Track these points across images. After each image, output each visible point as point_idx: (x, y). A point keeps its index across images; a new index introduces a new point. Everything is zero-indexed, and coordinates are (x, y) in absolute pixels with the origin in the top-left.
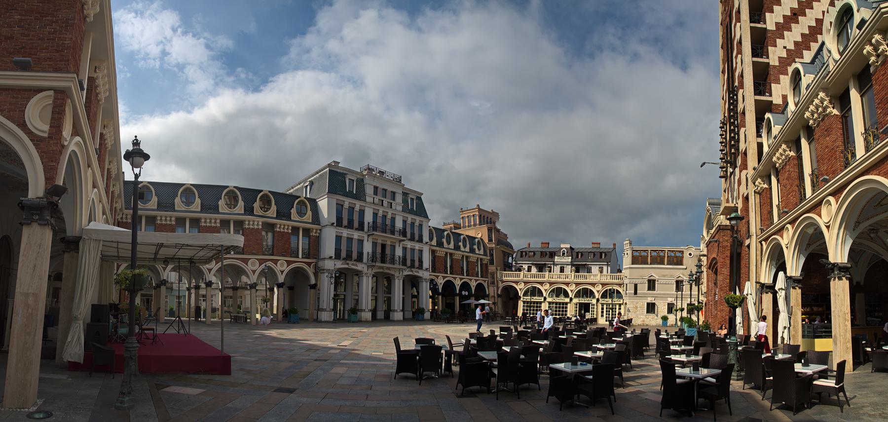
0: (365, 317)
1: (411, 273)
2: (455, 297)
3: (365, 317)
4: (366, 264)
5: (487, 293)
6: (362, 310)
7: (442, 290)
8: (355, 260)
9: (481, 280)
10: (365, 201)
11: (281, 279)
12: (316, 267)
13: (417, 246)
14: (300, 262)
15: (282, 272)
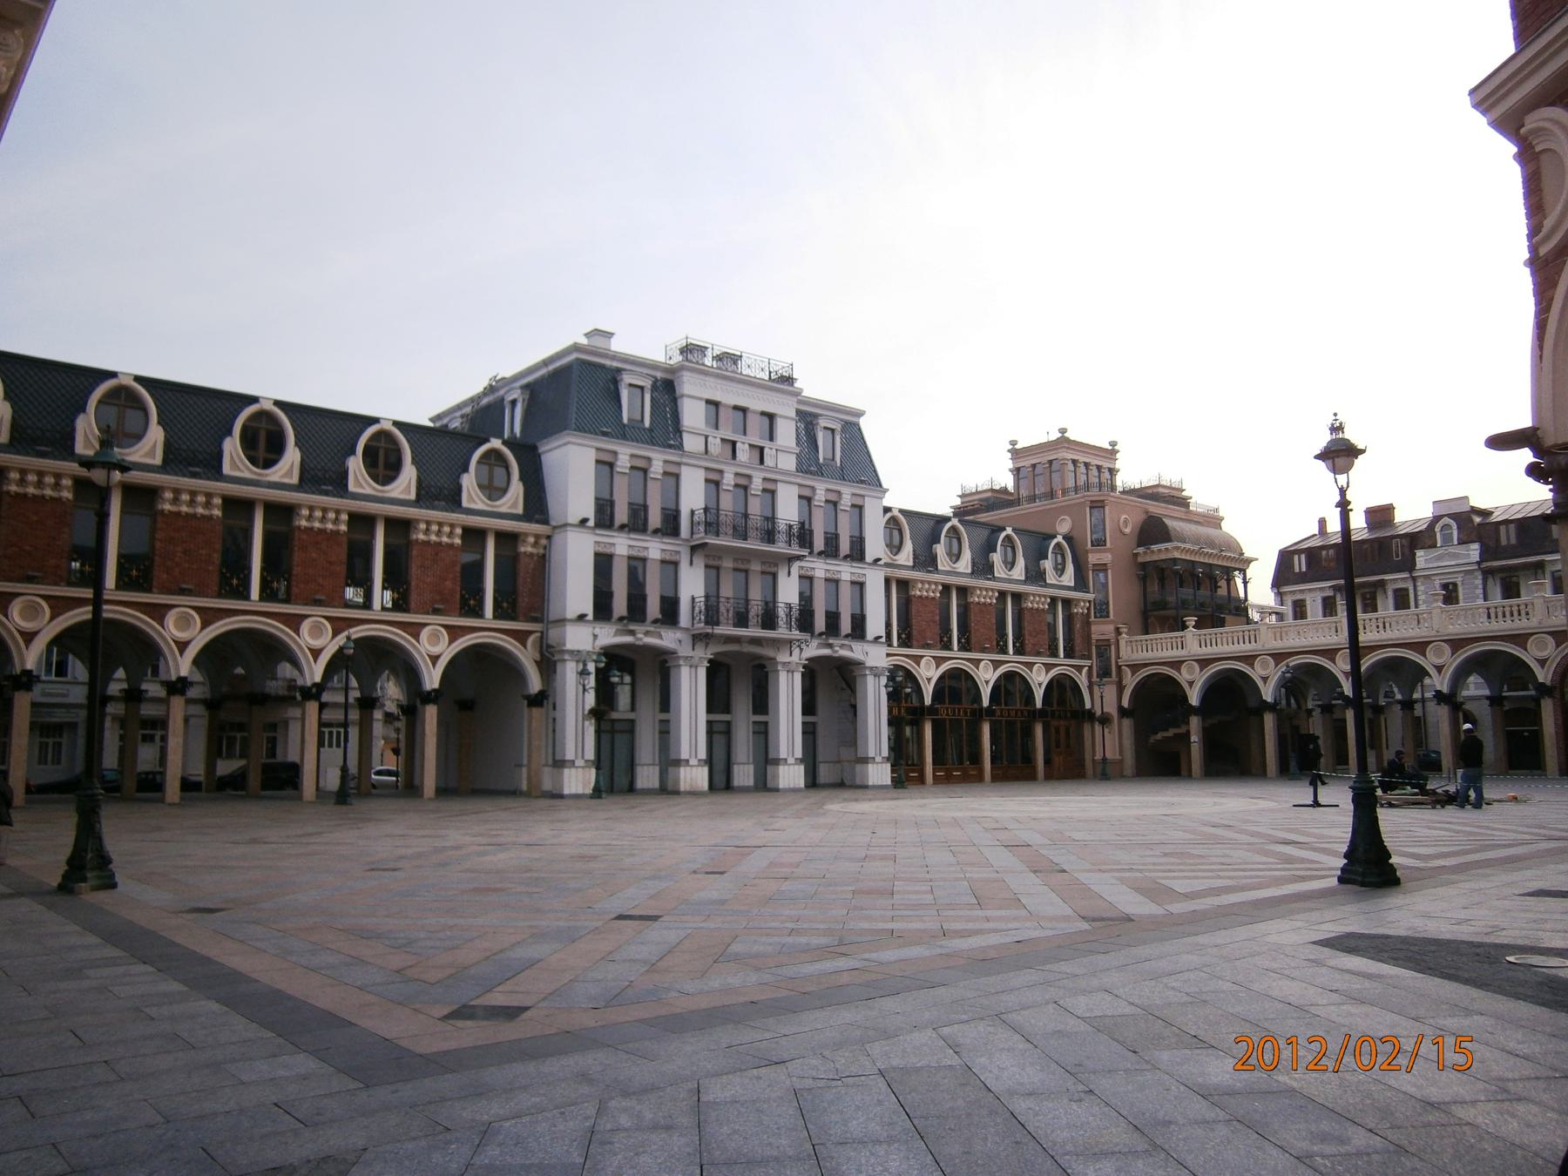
0: (688, 780)
1: (826, 652)
3: (688, 780)
4: (687, 629)
6: (868, 758)
7: (933, 700)
8: (655, 621)
9: (1063, 665)
10: (680, 447)
11: (432, 679)
12: (541, 647)
13: (846, 571)
14: (488, 630)
15: (435, 659)
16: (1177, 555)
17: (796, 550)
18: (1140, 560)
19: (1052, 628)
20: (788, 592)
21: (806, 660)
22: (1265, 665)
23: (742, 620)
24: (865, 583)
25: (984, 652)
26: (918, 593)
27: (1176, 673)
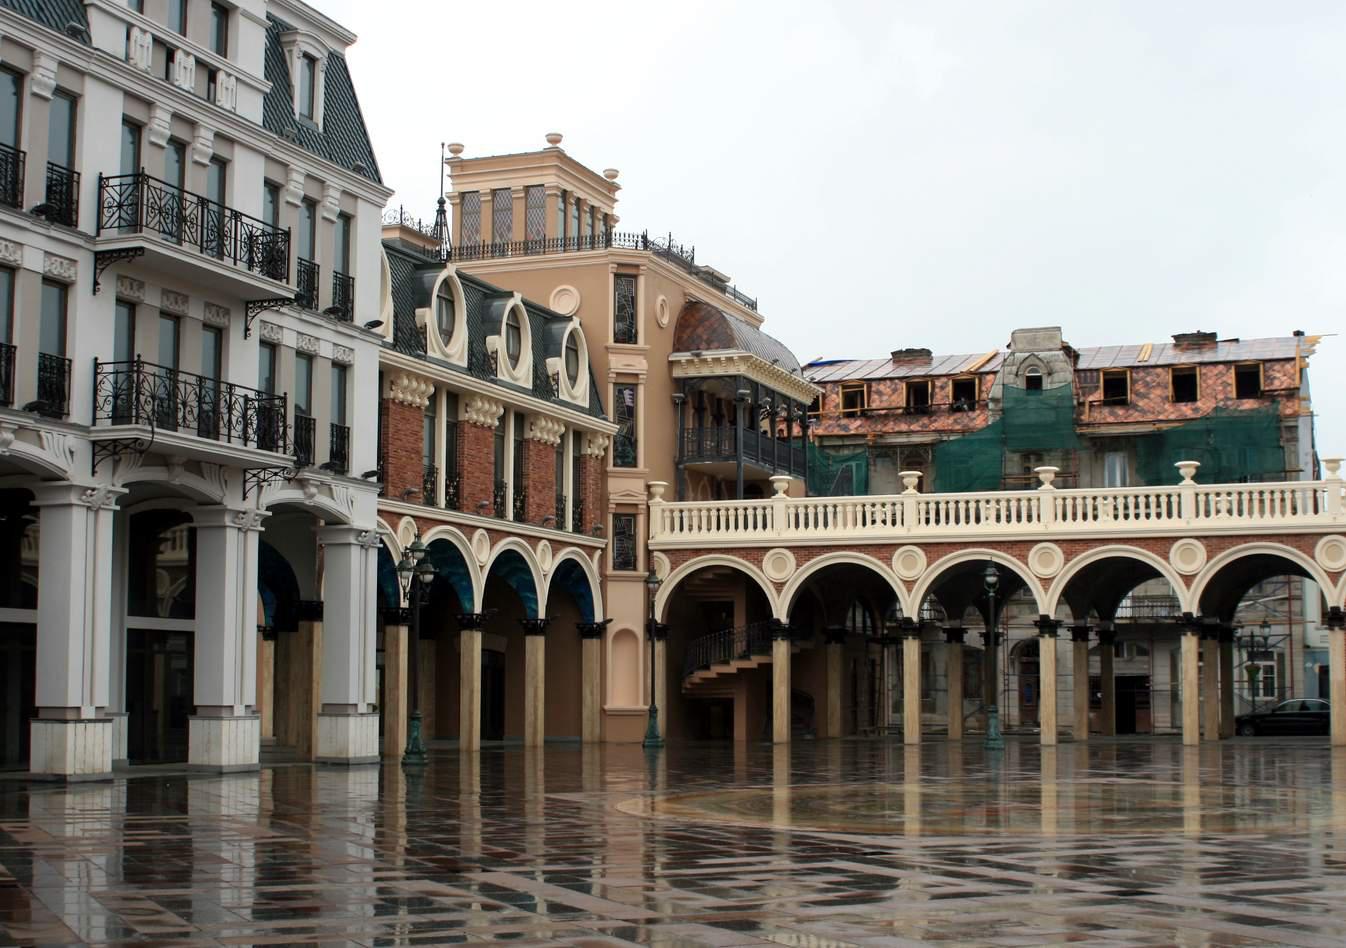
2: (465, 635)
5: (598, 618)
13: (327, 341)
18: (678, 373)
20: (244, 369)
21: (268, 509)
22: (780, 564)
23: (167, 418)
24: (351, 366)
25: (478, 514)
27: (755, 568)
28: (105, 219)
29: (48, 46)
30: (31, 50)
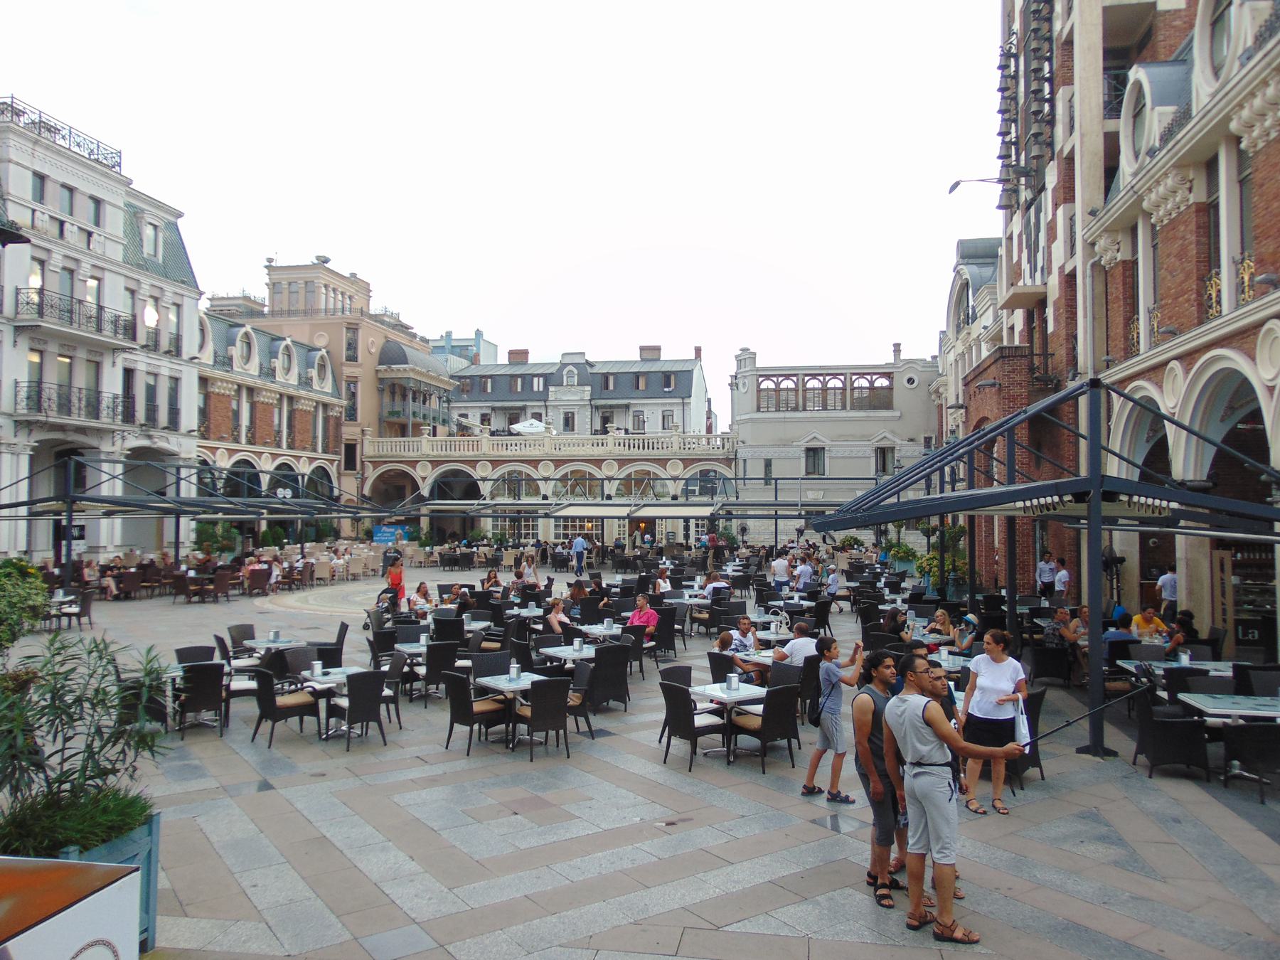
13: (166, 367)
16: (412, 375)
17: (121, 341)
18: (380, 375)
19: (236, 414)
24: (180, 378)
26: (217, 390)
28: (19, 310)
29: (788, 510)
30: (49, 251)
